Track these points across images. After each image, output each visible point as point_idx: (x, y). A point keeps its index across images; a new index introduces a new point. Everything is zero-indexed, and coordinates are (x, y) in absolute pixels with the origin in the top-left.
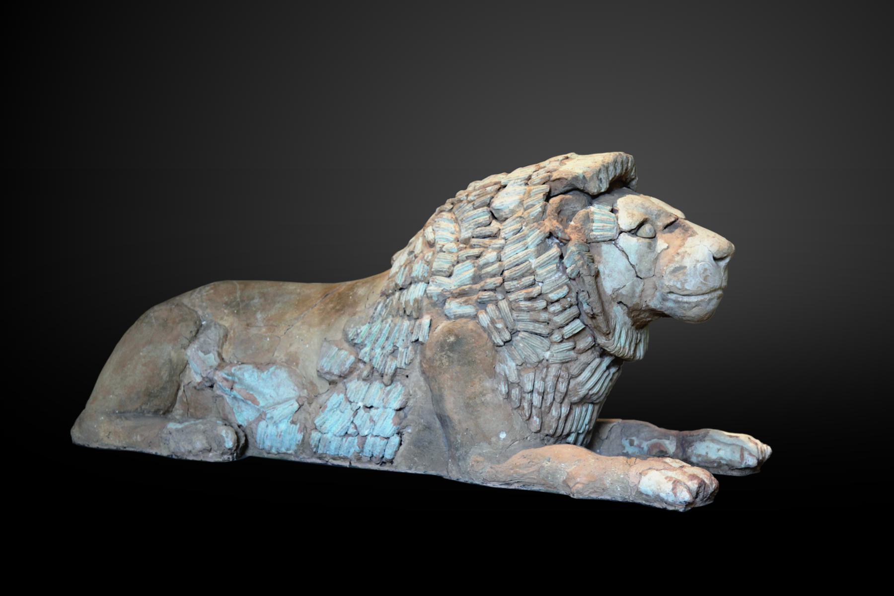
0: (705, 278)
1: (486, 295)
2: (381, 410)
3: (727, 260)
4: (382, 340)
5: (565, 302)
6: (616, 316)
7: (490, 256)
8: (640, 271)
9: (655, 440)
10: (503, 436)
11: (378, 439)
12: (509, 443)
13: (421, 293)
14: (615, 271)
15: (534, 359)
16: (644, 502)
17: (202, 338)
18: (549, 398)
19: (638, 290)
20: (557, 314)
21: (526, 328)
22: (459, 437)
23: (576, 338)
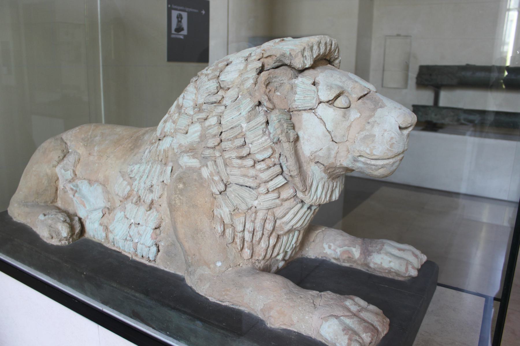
0: (391, 146)
1: (207, 152)
2: (144, 227)
4: (145, 177)
5: (270, 162)
6: (313, 174)
7: (213, 121)
8: (335, 136)
9: (346, 248)
10: (219, 264)
12: (224, 269)
13: (168, 145)
14: (316, 133)
15: (243, 207)
17: (66, 160)
18: (258, 235)
19: (333, 153)
22: (190, 258)
23: (280, 190)
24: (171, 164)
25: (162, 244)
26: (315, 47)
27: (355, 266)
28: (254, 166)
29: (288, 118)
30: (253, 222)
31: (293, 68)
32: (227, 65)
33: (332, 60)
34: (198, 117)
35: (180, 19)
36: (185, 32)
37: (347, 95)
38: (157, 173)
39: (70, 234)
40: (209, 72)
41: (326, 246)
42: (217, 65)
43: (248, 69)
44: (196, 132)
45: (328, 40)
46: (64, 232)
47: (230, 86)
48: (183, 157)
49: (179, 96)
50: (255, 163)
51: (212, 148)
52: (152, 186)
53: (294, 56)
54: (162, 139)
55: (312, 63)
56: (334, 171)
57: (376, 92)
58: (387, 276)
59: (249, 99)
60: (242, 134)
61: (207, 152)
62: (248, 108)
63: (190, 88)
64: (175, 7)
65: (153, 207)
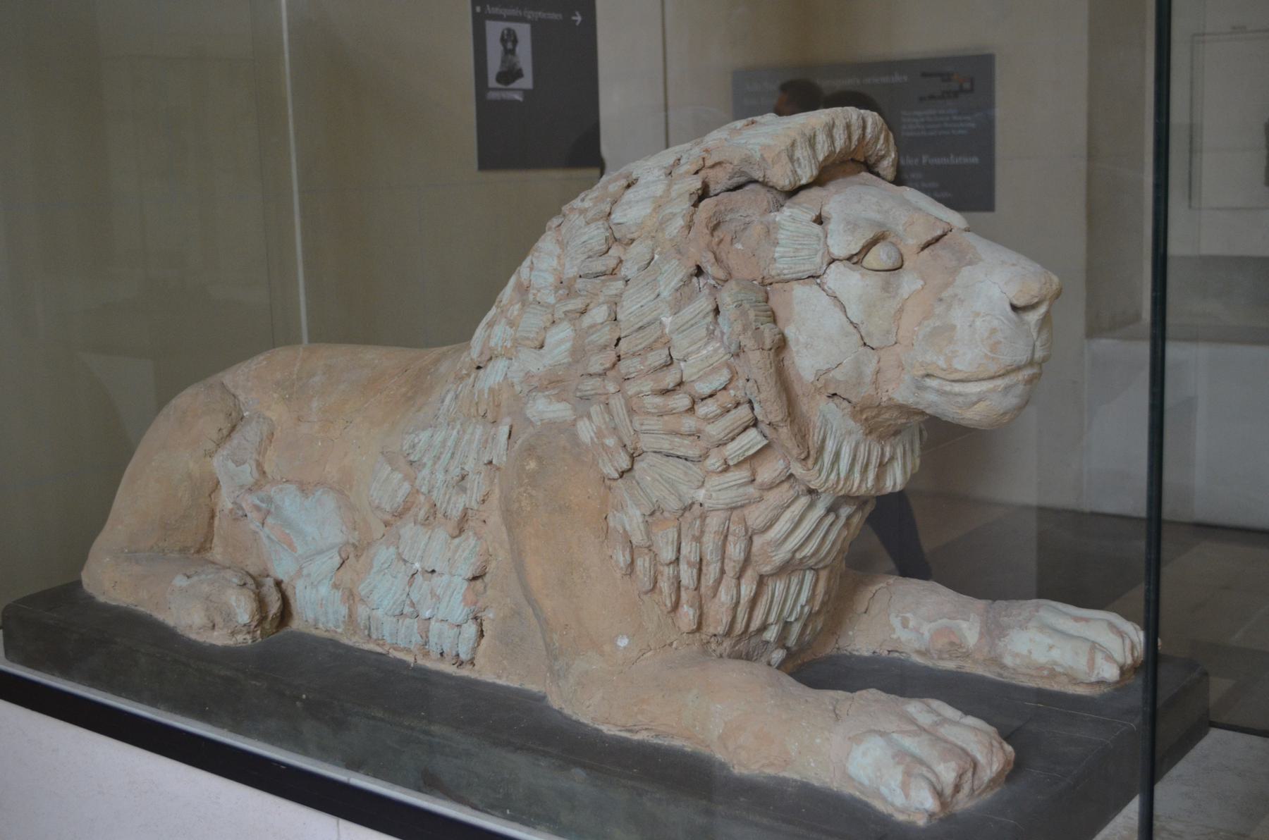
0: (994, 347)
1: (589, 385)
2: (445, 578)
3: (1042, 309)
4: (446, 456)
5: (725, 399)
6: (826, 422)
7: (599, 314)
9: (945, 621)
11: (446, 626)
13: (500, 378)
14: (820, 332)
15: (673, 504)
16: (857, 793)
19: (869, 370)
20: (710, 420)
21: (656, 446)
22: (555, 637)
24: (508, 420)
25: (489, 615)
26: (821, 138)
27: (970, 667)
28: (691, 410)
29: (761, 297)
30: (698, 539)
31: (772, 187)
32: (629, 186)
33: (873, 160)
34: (565, 309)
35: (510, 46)
36: (526, 82)
37: (894, 240)
38: (474, 446)
39: (257, 617)
40: (587, 204)
41: (896, 622)
42: (605, 188)
43: (673, 194)
44: (562, 342)
45: (855, 117)
46: (243, 610)
47: (634, 236)
48: (534, 400)
49: (520, 264)
50: (694, 402)
51: (600, 375)
52: (463, 478)
53: (770, 161)
54: (486, 366)
55: (815, 173)
56: (878, 415)
57: (967, 230)
58: (1047, 687)
59: (675, 262)
60: (663, 340)
61: (589, 385)
62: (675, 282)
63: (547, 243)
64: (496, 10)
65: (466, 526)
